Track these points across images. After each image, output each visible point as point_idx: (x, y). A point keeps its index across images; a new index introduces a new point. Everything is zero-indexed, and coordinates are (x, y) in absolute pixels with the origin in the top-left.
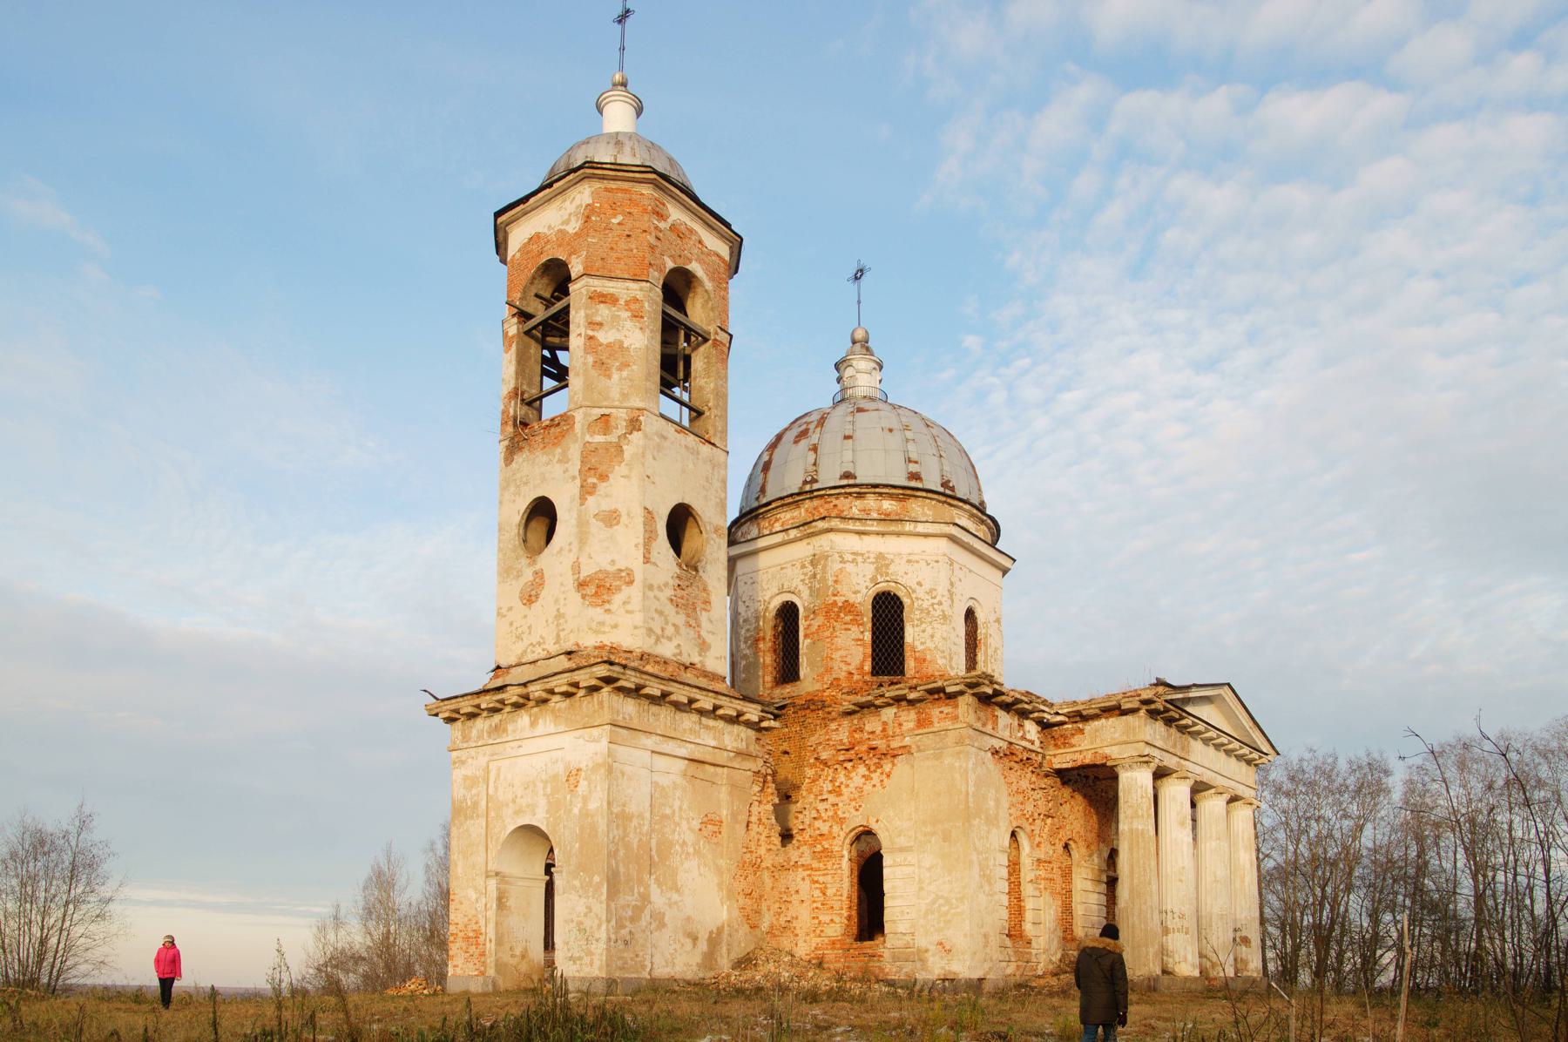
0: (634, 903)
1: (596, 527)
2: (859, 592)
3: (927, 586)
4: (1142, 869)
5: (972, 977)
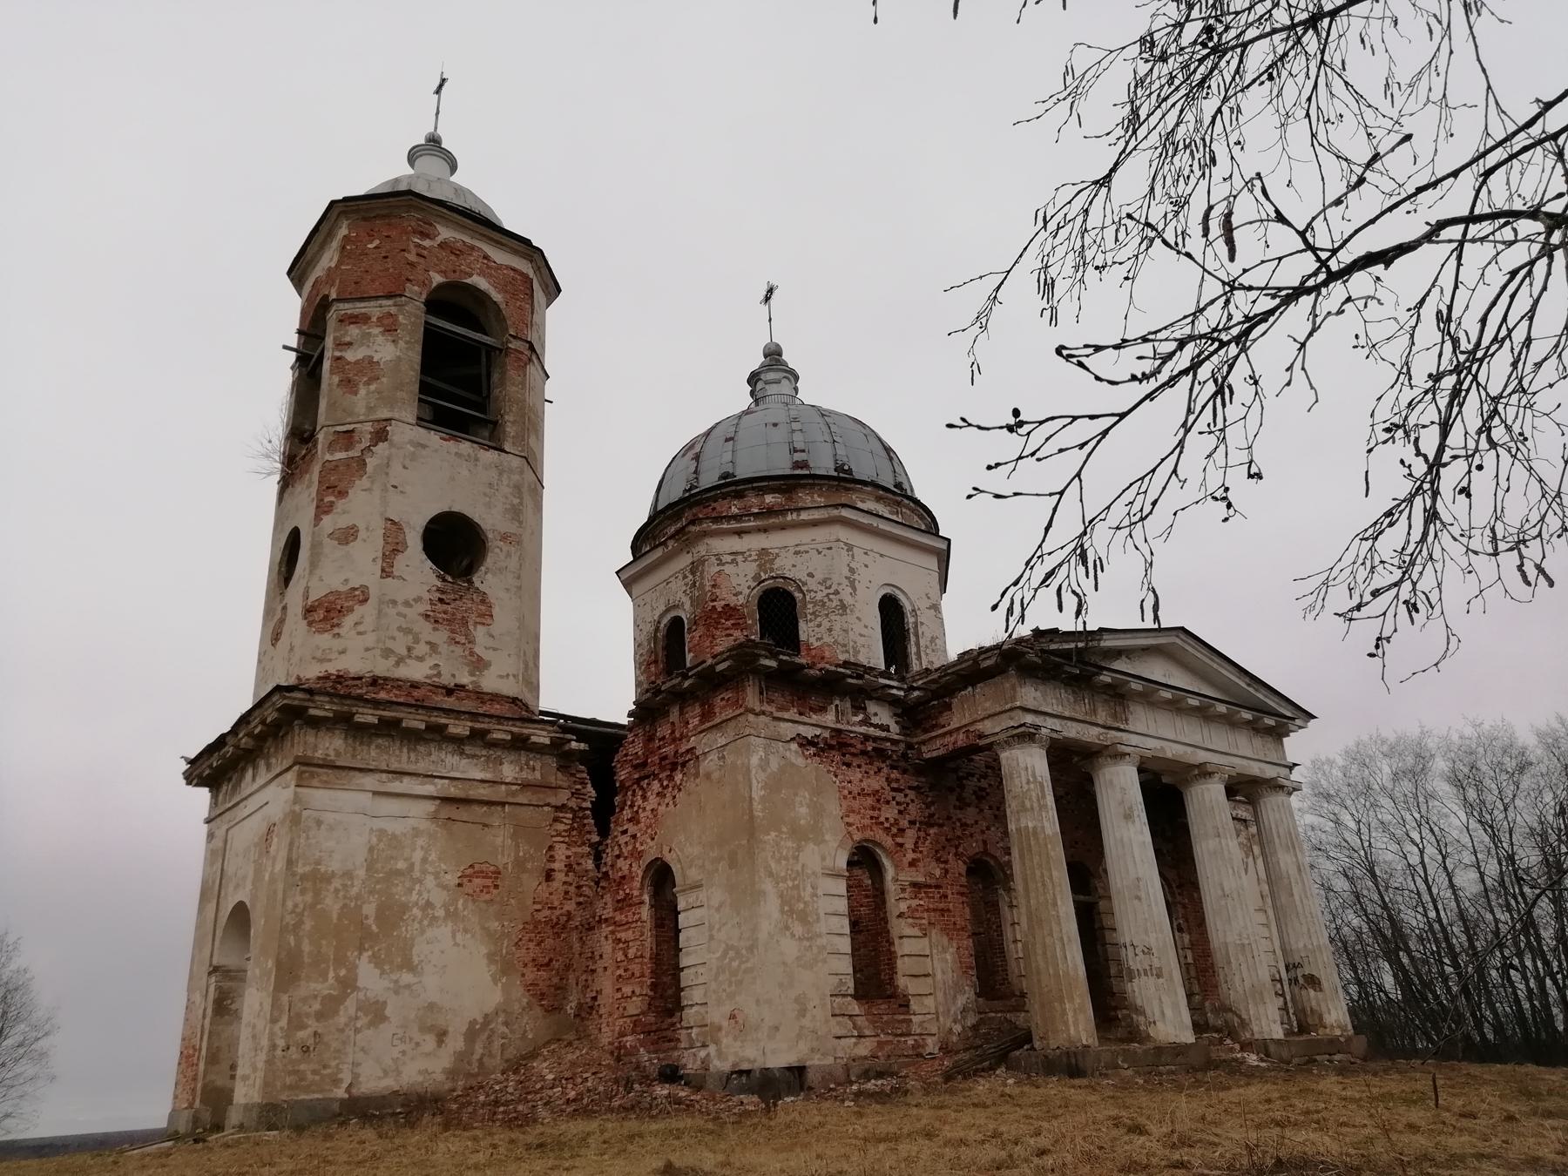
0: (326, 992)
1: (329, 545)
2: (741, 593)
3: (819, 576)
4: (1039, 885)
5: (769, 1065)
